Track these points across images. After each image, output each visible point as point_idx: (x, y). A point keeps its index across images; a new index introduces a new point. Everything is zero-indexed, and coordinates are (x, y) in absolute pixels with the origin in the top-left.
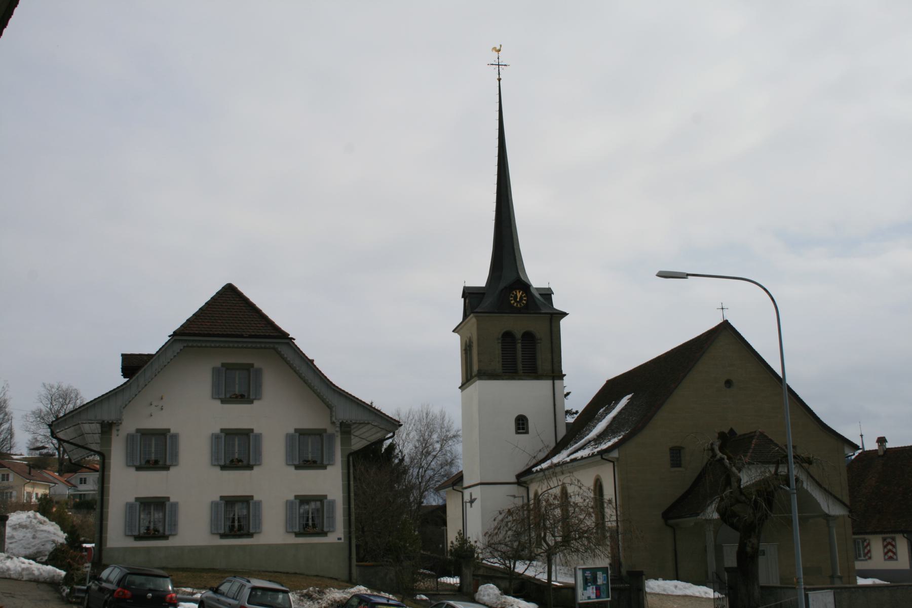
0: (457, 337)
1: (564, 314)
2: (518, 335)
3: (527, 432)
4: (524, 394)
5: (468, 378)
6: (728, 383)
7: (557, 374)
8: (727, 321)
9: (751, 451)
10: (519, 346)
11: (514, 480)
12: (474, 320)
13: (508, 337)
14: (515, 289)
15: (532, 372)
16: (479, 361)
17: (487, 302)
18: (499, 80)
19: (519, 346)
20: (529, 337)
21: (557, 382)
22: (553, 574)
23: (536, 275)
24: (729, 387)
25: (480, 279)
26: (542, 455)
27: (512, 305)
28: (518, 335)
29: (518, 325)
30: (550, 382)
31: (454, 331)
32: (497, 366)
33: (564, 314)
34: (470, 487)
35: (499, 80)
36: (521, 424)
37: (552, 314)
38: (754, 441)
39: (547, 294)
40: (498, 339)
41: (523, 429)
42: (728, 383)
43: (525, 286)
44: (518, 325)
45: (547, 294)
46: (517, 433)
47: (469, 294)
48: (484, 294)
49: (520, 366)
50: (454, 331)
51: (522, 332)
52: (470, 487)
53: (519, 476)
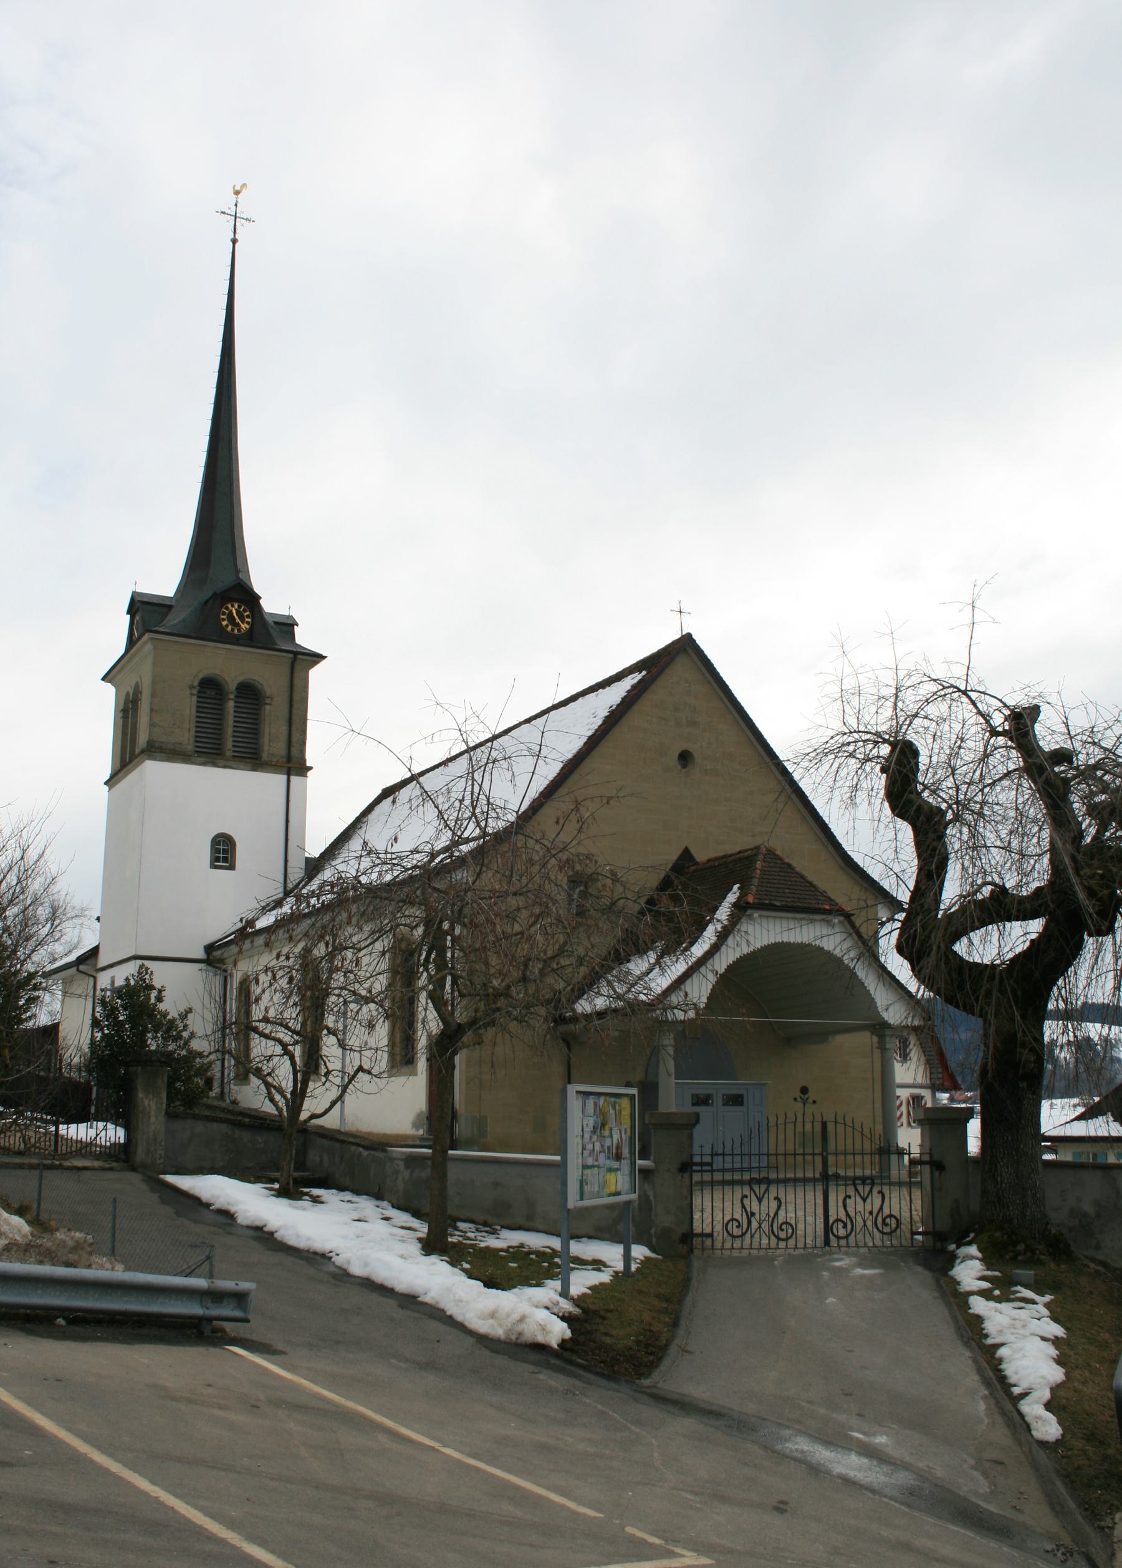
0: (110, 690)
1: (319, 657)
2: (232, 686)
3: (232, 867)
4: (232, 795)
5: (127, 757)
6: (685, 758)
7: (294, 764)
8: (689, 635)
9: (755, 881)
10: (231, 704)
11: (200, 954)
12: (149, 647)
13: (210, 689)
14: (232, 600)
15: (251, 757)
16: (152, 725)
17: (174, 620)
18: (234, 241)
19: (231, 704)
20: (250, 693)
21: (293, 778)
22: (878, 1075)
23: (279, 574)
24: (684, 766)
25: (165, 579)
26: (87, 1174)
27: (223, 629)
28: (232, 686)
29: (233, 665)
30: (283, 778)
31: (103, 679)
32: (186, 737)
33: (319, 657)
34: (111, 966)
35: (234, 241)
36: (223, 851)
37: (296, 654)
38: (759, 864)
39: (287, 626)
40: (192, 687)
41: (225, 860)
42: (685, 758)
43: (251, 600)
44: (233, 665)
45: (287, 626)
46: (213, 866)
47: (145, 612)
48: (170, 607)
49: (229, 744)
50: (103, 679)
51: (240, 679)
52: (111, 966)
53: (210, 948)
